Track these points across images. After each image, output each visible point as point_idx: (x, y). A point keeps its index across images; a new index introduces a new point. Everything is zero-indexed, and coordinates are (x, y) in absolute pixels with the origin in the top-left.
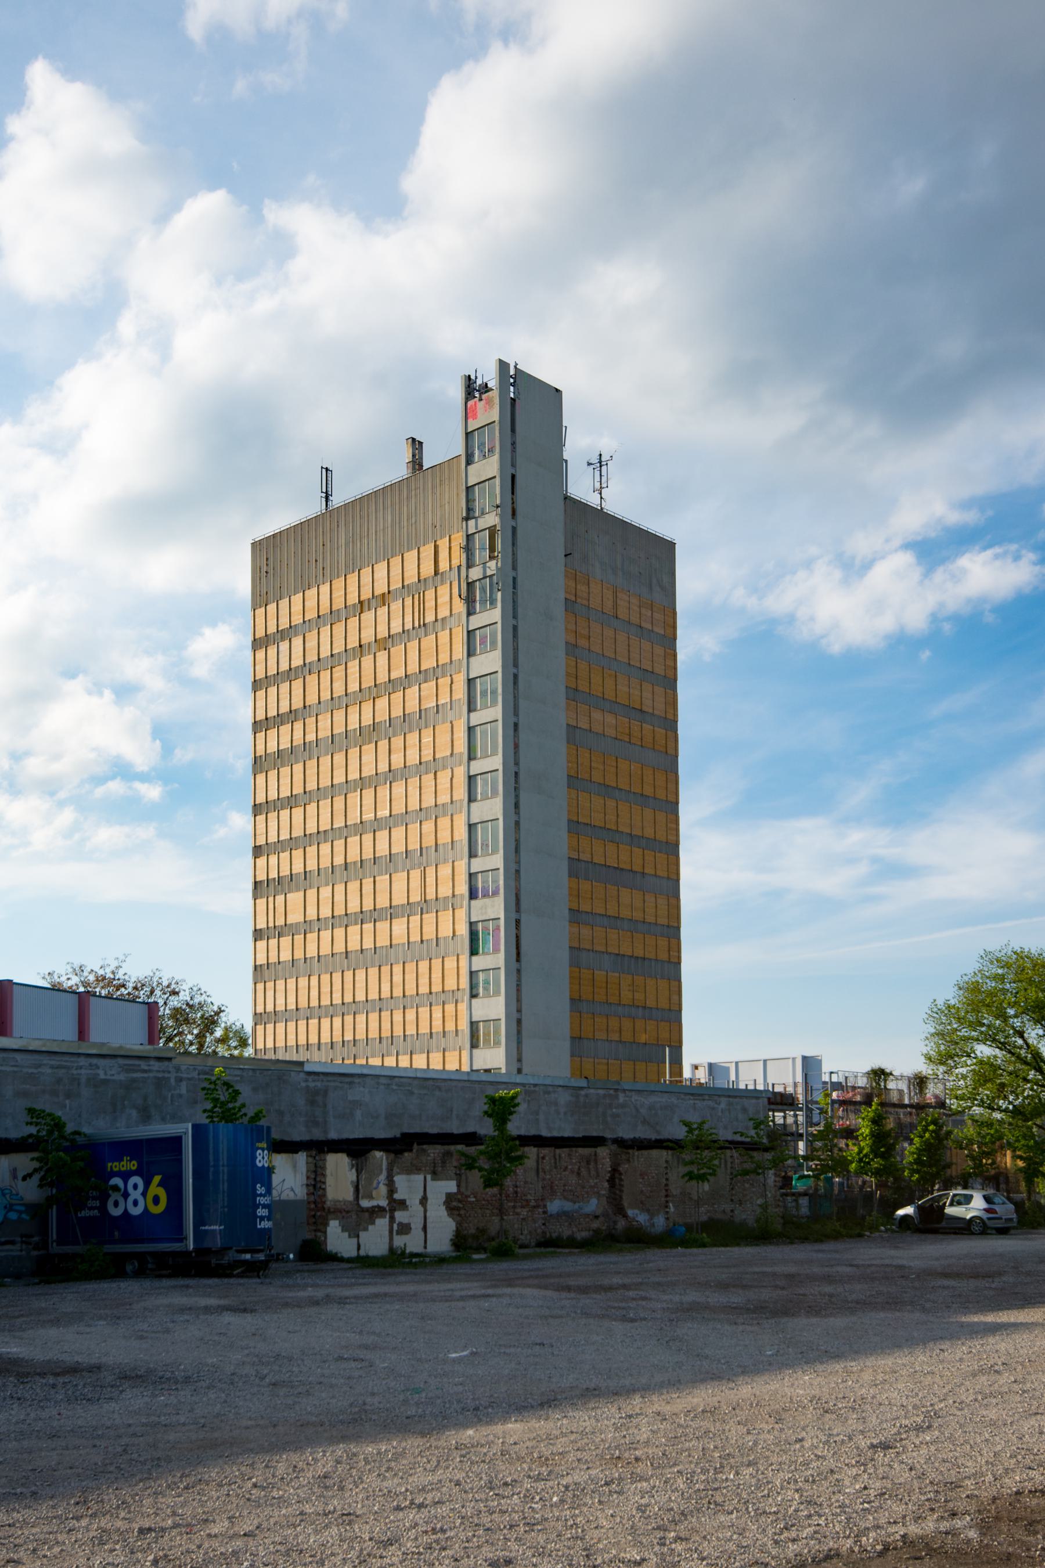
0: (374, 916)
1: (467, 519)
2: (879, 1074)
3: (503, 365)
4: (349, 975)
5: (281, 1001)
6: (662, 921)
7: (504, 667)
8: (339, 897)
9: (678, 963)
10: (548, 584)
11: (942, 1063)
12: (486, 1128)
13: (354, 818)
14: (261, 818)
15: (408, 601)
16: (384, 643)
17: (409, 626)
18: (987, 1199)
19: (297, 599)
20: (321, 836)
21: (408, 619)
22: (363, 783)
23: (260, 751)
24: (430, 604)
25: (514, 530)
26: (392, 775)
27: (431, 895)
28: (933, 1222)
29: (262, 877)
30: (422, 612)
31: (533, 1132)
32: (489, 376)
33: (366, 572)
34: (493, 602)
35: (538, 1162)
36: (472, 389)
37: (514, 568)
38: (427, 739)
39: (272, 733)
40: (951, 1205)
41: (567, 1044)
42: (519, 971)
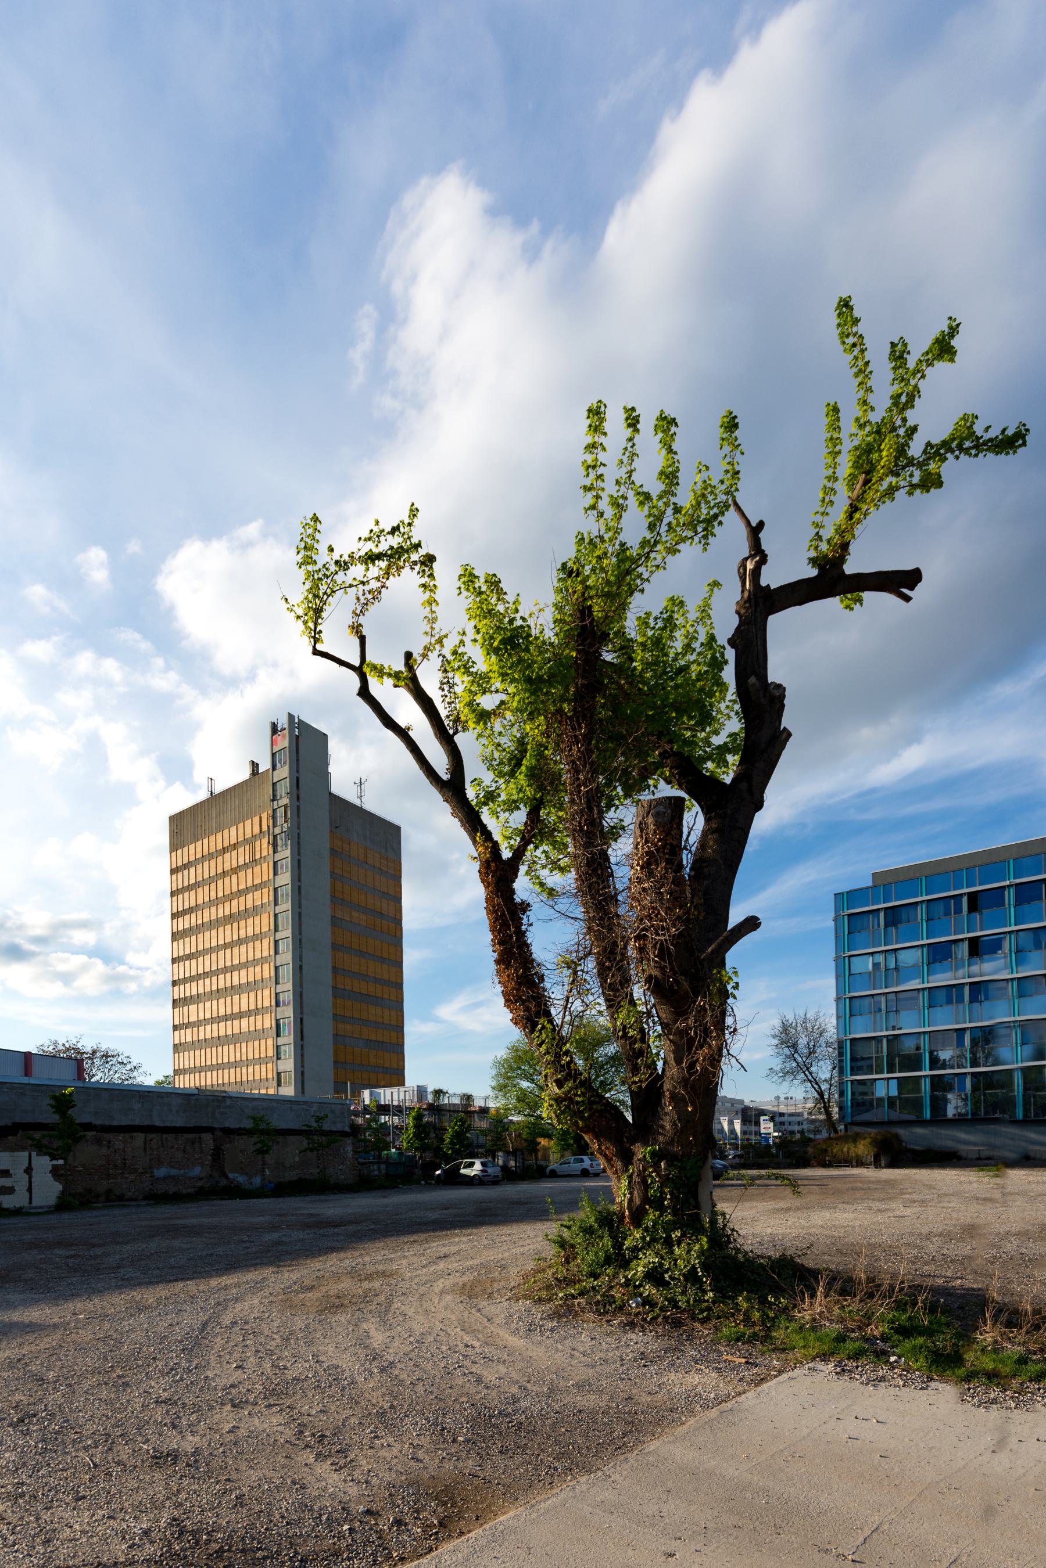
0: (232, 1017)
1: (273, 800)
2: (468, 1098)
3: (291, 717)
4: (220, 1049)
5: (187, 1063)
6: (394, 1023)
7: (292, 881)
8: (215, 1007)
9: (403, 1045)
10: (320, 839)
11: (501, 1090)
12: (54, 1118)
13: (221, 965)
14: (176, 965)
15: (247, 847)
16: (235, 870)
17: (247, 861)
18: (483, 1164)
19: (192, 847)
20: (205, 975)
21: (247, 857)
22: (226, 946)
23: (175, 930)
24: (258, 849)
25: (298, 807)
26: (240, 942)
27: (260, 1006)
28: (454, 1179)
29: (176, 997)
30: (254, 854)
31: (146, 1123)
32: (283, 722)
33: (226, 831)
34: (286, 846)
35: (145, 1143)
36: (274, 729)
37: (299, 828)
38: (257, 922)
39: (181, 920)
40: (465, 1167)
41: (332, 1085)
42: (302, 1046)
